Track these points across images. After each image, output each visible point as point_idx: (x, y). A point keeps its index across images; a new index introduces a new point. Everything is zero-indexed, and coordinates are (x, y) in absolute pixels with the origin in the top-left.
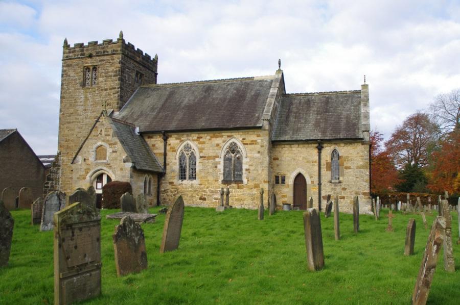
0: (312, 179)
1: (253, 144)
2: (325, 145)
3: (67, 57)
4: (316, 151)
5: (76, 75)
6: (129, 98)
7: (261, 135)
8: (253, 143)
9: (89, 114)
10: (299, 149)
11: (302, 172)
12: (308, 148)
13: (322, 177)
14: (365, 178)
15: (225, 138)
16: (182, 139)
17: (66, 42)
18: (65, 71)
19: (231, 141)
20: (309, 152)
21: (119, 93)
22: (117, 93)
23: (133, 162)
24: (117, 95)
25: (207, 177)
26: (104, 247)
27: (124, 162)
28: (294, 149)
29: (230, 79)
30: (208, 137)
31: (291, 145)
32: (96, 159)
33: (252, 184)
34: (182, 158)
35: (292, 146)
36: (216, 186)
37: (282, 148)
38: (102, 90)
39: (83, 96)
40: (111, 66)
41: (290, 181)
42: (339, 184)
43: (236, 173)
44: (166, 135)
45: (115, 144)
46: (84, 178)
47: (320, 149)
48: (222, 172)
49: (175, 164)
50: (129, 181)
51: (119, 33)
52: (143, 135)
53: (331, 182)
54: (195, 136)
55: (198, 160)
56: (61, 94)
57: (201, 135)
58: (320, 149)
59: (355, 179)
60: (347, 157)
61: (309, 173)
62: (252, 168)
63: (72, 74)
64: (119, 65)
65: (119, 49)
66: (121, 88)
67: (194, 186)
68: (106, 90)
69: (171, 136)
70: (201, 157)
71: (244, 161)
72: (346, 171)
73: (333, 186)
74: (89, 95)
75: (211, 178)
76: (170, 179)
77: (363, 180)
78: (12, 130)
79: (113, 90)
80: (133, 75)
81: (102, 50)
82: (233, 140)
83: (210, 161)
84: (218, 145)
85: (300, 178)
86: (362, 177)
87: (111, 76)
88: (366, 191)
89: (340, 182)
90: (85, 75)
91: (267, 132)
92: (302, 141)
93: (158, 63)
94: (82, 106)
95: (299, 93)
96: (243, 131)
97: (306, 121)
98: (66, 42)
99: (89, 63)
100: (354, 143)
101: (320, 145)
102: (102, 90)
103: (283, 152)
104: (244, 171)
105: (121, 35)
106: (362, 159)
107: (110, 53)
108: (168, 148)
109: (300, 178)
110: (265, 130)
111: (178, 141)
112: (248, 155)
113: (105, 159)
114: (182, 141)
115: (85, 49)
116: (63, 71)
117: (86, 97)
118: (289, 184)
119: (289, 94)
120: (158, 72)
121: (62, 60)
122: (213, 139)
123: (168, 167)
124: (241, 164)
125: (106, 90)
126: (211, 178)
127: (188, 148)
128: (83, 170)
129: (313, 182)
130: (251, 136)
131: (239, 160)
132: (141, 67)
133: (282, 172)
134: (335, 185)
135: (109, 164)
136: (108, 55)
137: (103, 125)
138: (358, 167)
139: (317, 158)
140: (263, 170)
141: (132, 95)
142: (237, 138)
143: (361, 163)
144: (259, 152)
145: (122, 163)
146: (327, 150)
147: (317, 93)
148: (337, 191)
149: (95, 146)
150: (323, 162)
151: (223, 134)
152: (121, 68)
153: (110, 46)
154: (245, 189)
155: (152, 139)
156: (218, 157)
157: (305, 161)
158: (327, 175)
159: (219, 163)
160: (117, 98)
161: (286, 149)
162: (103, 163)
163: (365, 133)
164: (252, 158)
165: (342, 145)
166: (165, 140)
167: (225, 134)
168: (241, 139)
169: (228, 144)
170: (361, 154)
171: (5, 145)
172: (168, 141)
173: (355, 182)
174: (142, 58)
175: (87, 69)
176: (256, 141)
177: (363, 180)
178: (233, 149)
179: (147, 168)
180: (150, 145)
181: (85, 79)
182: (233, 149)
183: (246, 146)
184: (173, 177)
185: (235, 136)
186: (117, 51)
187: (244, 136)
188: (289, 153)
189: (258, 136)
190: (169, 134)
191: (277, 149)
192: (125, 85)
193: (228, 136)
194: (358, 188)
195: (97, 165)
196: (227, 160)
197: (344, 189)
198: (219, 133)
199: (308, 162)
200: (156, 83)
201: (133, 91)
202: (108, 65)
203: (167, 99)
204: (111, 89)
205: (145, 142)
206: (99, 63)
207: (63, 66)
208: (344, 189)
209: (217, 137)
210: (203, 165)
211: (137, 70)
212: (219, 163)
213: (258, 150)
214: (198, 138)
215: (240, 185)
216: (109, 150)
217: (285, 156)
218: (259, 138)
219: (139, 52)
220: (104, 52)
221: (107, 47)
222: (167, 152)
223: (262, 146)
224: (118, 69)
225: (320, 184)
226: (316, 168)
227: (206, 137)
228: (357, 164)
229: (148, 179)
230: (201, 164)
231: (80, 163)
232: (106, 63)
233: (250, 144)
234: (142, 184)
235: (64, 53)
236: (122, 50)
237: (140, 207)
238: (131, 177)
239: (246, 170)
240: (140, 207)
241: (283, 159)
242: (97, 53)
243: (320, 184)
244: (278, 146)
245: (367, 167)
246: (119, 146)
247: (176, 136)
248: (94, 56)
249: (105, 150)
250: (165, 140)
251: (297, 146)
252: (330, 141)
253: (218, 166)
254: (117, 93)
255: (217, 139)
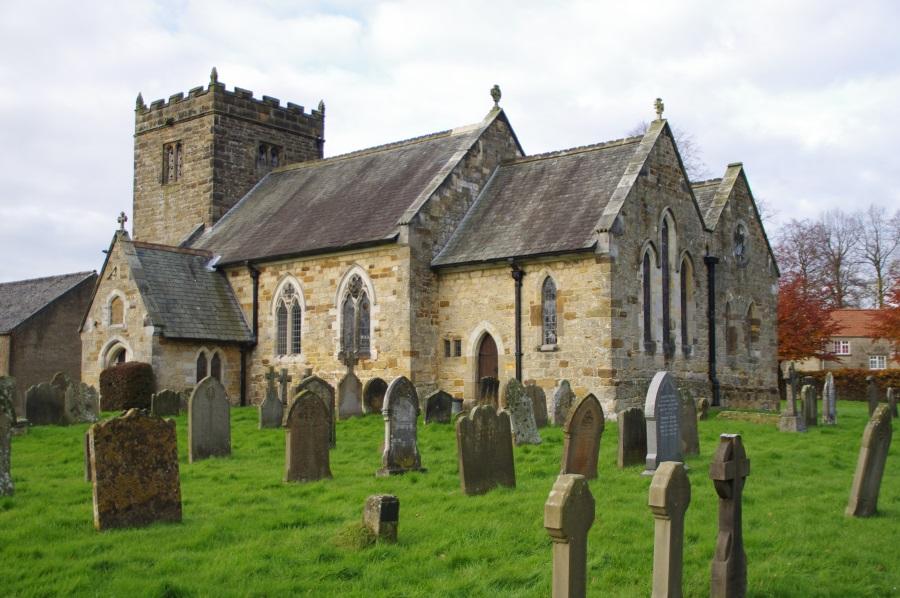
0: (507, 345)
1: (385, 276)
2: (528, 269)
3: (141, 129)
4: (513, 282)
5: (154, 164)
6: (239, 197)
7: (399, 256)
8: (387, 272)
9: (171, 234)
10: (484, 280)
11: (491, 333)
12: (499, 278)
13: (522, 338)
14: (602, 338)
15: (343, 267)
16: (281, 273)
17: (140, 101)
18: (139, 156)
19: (351, 274)
20: (500, 285)
21: (212, 191)
22: (209, 190)
23: (156, 326)
24: (208, 195)
25: (316, 348)
26: (520, 472)
27: (145, 325)
28: (475, 281)
29: (411, 140)
30: (318, 268)
31: (469, 272)
32: (111, 322)
33: (384, 359)
34: (282, 312)
35: (472, 274)
36: (330, 366)
37: (455, 280)
38: (188, 187)
39: (162, 202)
40: (201, 138)
41: (470, 349)
42: (555, 353)
43: (362, 337)
44: (255, 269)
45: (133, 292)
46: (96, 359)
47: (519, 277)
48: (339, 336)
49: (270, 324)
50: (150, 362)
51: (210, 73)
52: (226, 270)
53: (539, 350)
54: (298, 266)
55: (304, 315)
56: (134, 200)
57: (307, 264)
58: (519, 277)
59: (583, 341)
60: (570, 292)
61: (500, 331)
62: (384, 326)
63: (147, 161)
64: (211, 136)
65: (211, 103)
66: (215, 180)
67: (298, 366)
68: (193, 186)
69: (264, 270)
70: (307, 308)
71: (374, 310)
72: (567, 323)
73: (543, 360)
74: (171, 200)
75: (322, 350)
76: (264, 354)
77: (599, 342)
78: (85, 274)
79: (204, 186)
80: (252, 151)
81: (187, 110)
82: (356, 270)
83: (321, 315)
84: (332, 282)
85: (486, 340)
86: (596, 334)
87: (199, 159)
88: (604, 368)
89: (556, 349)
90: (166, 160)
91: (407, 250)
92: (481, 262)
93: (326, 119)
94: (162, 220)
95: (533, 155)
96: (371, 250)
97: (515, 218)
98: (140, 101)
99: (169, 137)
100: (582, 260)
101: (517, 267)
102: (188, 187)
103: (456, 289)
104: (372, 333)
105: (214, 76)
106: (597, 295)
107: (198, 113)
108: (260, 292)
109: (486, 340)
110: (403, 246)
111: (274, 279)
112: (379, 299)
113: (122, 322)
114: (280, 279)
115: (165, 110)
116: (137, 157)
117: (167, 204)
118: (467, 355)
119: (531, 157)
120: (325, 138)
121: (135, 136)
122: (326, 270)
123: (260, 330)
124: (367, 317)
125: (193, 186)
126: (322, 350)
127: (289, 290)
128: (94, 343)
129: (507, 351)
130: (384, 260)
131: (365, 306)
132: (274, 132)
133: (455, 332)
134: (548, 356)
135: (126, 331)
136: (195, 118)
137: (118, 258)
138: (591, 314)
139: (512, 298)
140: (401, 329)
141: (249, 190)
142: (361, 266)
143: (595, 304)
144: (394, 293)
145: (142, 328)
146: (534, 279)
147: (566, 151)
148: (551, 369)
149: (109, 298)
150: (526, 306)
151: (341, 259)
152: (215, 140)
153: (198, 99)
154: (374, 369)
155: (239, 278)
156: (330, 306)
157: (495, 305)
158: (532, 334)
159: (333, 318)
160: (208, 201)
161: (462, 281)
162: (118, 329)
163: (602, 235)
164: (385, 305)
165: (560, 265)
166: (256, 276)
167: (344, 258)
168: (367, 267)
169: (348, 279)
170: (595, 284)
171: (72, 302)
172: (260, 280)
173: (583, 347)
174: (276, 114)
175: (167, 147)
176: (390, 269)
177: (599, 342)
178: (356, 288)
179: (203, 335)
180: (236, 289)
181: (166, 169)
182: (356, 288)
183: (374, 280)
184: (267, 351)
185: (357, 262)
186: (208, 108)
187: (371, 261)
188: (467, 290)
189: (394, 258)
190: (262, 265)
191: (447, 283)
192: (227, 173)
193: (349, 263)
194: (590, 361)
195: (111, 332)
196: (347, 310)
197: (564, 364)
198: (334, 258)
199: (498, 308)
200: (320, 154)
201: (252, 183)
202: (196, 137)
203: (294, 195)
204: (200, 184)
205: (228, 283)
206: (184, 136)
207: (136, 148)
208: (564, 364)
209: (331, 266)
210: (310, 323)
211: (261, 138)
212: (333, 318)
213: (393, 287)
214: (303, 270)
215: (366, 361)
216: (127, 305)
217: (460, 296)
218: (395, 263)
219: (270, 103)
220: (190, 112)
221: (194, 101)
222: (259, 301)
223: (399, 280)
224: (209, 143)
225: (519, 355)
226: (513, 319)
227: (315, 266)
228: (589, 306)
229: (210, 356)
230: (307, 322)
231: (90, 331)
232: (194, 133)
233: (383, 276)
234: (193, 366)
235: (137, 123)
236: (215, 106)
237: (74, 409)
238: (155, 352)
239: (376, 330)
240: (74, 409)
241: (457, 303)
242: (181, 116)
243: (519, 355)
244: (449, 277)
245: (606, 313)
246: (138, 297)
247: (271, 269)
248: (177, 123)
249: (121, 304)
250: (256, 276)
251: (479, 273)
252: (536, 258)
253: (333, 324)
254: (209, 190)
255: (332, 270)
